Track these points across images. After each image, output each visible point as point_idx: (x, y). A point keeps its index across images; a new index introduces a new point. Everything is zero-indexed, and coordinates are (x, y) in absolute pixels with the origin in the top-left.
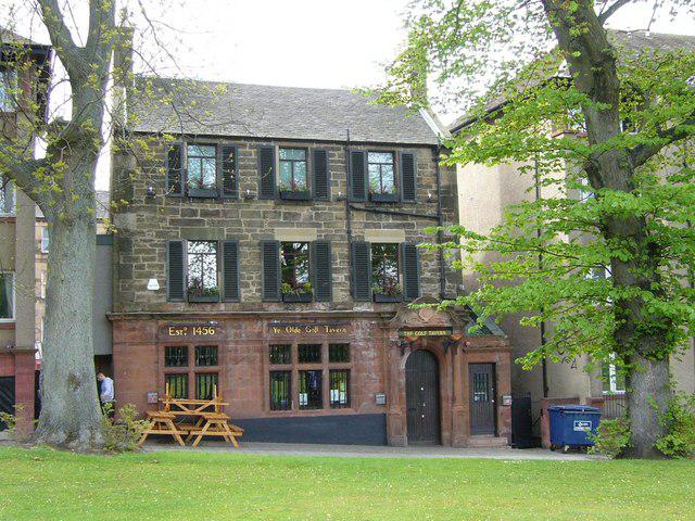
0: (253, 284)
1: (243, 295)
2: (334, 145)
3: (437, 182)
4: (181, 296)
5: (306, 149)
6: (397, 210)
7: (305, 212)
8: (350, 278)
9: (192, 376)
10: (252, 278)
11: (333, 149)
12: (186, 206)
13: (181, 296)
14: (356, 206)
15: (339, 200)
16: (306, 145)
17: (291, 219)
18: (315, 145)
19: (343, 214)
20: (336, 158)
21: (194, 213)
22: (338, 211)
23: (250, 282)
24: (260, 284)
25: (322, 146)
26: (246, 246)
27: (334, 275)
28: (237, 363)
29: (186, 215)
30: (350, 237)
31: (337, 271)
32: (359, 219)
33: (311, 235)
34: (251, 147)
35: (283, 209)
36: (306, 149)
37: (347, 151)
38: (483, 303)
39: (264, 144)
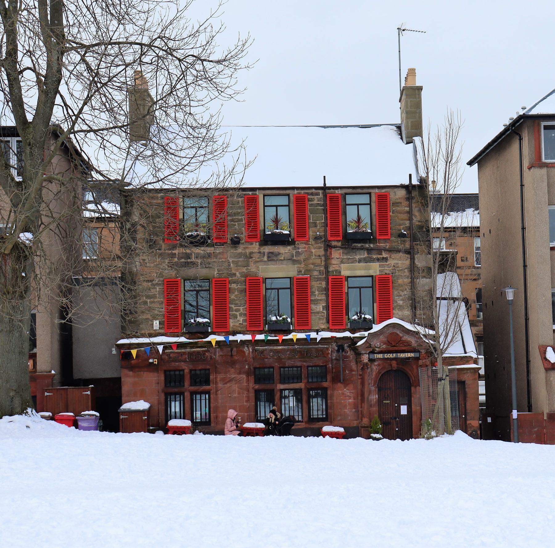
0: (241, 315)
1: (231, 325)
2: (314, 191)
3: (410, 219)
4: (340, 381)
5: (288, 195)
6: (372, 246)
7: (285, 250)
8: (327, 308)
9: (187, 394)
10: (239, 310)
11: (312, 194)
12: (182, 250)
13: (340, 381)
14: (334, 243)
15: (316, 238)
16: (288, 192)
17: (272, 257)
18: (296, 192)
19: (322, 252)
20: (316, 202)
21: (188, 256)
22: (317, 250)
23: (238, 313)
24: (245, 315)
25: (303, 192)
26: (234, 283)
27: (313, 307)
28: (226, 383)
29: (182, 258)
30: (327, 272)
31: (316, 302)
32: (336, 254)
33: (292, 271)
34: (238, 196)
35: (267, 249)
36: (288, 195)
37: (325, 195)
38: (174, 271)
39: (250, 193)
